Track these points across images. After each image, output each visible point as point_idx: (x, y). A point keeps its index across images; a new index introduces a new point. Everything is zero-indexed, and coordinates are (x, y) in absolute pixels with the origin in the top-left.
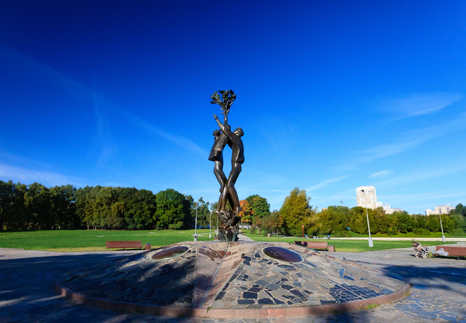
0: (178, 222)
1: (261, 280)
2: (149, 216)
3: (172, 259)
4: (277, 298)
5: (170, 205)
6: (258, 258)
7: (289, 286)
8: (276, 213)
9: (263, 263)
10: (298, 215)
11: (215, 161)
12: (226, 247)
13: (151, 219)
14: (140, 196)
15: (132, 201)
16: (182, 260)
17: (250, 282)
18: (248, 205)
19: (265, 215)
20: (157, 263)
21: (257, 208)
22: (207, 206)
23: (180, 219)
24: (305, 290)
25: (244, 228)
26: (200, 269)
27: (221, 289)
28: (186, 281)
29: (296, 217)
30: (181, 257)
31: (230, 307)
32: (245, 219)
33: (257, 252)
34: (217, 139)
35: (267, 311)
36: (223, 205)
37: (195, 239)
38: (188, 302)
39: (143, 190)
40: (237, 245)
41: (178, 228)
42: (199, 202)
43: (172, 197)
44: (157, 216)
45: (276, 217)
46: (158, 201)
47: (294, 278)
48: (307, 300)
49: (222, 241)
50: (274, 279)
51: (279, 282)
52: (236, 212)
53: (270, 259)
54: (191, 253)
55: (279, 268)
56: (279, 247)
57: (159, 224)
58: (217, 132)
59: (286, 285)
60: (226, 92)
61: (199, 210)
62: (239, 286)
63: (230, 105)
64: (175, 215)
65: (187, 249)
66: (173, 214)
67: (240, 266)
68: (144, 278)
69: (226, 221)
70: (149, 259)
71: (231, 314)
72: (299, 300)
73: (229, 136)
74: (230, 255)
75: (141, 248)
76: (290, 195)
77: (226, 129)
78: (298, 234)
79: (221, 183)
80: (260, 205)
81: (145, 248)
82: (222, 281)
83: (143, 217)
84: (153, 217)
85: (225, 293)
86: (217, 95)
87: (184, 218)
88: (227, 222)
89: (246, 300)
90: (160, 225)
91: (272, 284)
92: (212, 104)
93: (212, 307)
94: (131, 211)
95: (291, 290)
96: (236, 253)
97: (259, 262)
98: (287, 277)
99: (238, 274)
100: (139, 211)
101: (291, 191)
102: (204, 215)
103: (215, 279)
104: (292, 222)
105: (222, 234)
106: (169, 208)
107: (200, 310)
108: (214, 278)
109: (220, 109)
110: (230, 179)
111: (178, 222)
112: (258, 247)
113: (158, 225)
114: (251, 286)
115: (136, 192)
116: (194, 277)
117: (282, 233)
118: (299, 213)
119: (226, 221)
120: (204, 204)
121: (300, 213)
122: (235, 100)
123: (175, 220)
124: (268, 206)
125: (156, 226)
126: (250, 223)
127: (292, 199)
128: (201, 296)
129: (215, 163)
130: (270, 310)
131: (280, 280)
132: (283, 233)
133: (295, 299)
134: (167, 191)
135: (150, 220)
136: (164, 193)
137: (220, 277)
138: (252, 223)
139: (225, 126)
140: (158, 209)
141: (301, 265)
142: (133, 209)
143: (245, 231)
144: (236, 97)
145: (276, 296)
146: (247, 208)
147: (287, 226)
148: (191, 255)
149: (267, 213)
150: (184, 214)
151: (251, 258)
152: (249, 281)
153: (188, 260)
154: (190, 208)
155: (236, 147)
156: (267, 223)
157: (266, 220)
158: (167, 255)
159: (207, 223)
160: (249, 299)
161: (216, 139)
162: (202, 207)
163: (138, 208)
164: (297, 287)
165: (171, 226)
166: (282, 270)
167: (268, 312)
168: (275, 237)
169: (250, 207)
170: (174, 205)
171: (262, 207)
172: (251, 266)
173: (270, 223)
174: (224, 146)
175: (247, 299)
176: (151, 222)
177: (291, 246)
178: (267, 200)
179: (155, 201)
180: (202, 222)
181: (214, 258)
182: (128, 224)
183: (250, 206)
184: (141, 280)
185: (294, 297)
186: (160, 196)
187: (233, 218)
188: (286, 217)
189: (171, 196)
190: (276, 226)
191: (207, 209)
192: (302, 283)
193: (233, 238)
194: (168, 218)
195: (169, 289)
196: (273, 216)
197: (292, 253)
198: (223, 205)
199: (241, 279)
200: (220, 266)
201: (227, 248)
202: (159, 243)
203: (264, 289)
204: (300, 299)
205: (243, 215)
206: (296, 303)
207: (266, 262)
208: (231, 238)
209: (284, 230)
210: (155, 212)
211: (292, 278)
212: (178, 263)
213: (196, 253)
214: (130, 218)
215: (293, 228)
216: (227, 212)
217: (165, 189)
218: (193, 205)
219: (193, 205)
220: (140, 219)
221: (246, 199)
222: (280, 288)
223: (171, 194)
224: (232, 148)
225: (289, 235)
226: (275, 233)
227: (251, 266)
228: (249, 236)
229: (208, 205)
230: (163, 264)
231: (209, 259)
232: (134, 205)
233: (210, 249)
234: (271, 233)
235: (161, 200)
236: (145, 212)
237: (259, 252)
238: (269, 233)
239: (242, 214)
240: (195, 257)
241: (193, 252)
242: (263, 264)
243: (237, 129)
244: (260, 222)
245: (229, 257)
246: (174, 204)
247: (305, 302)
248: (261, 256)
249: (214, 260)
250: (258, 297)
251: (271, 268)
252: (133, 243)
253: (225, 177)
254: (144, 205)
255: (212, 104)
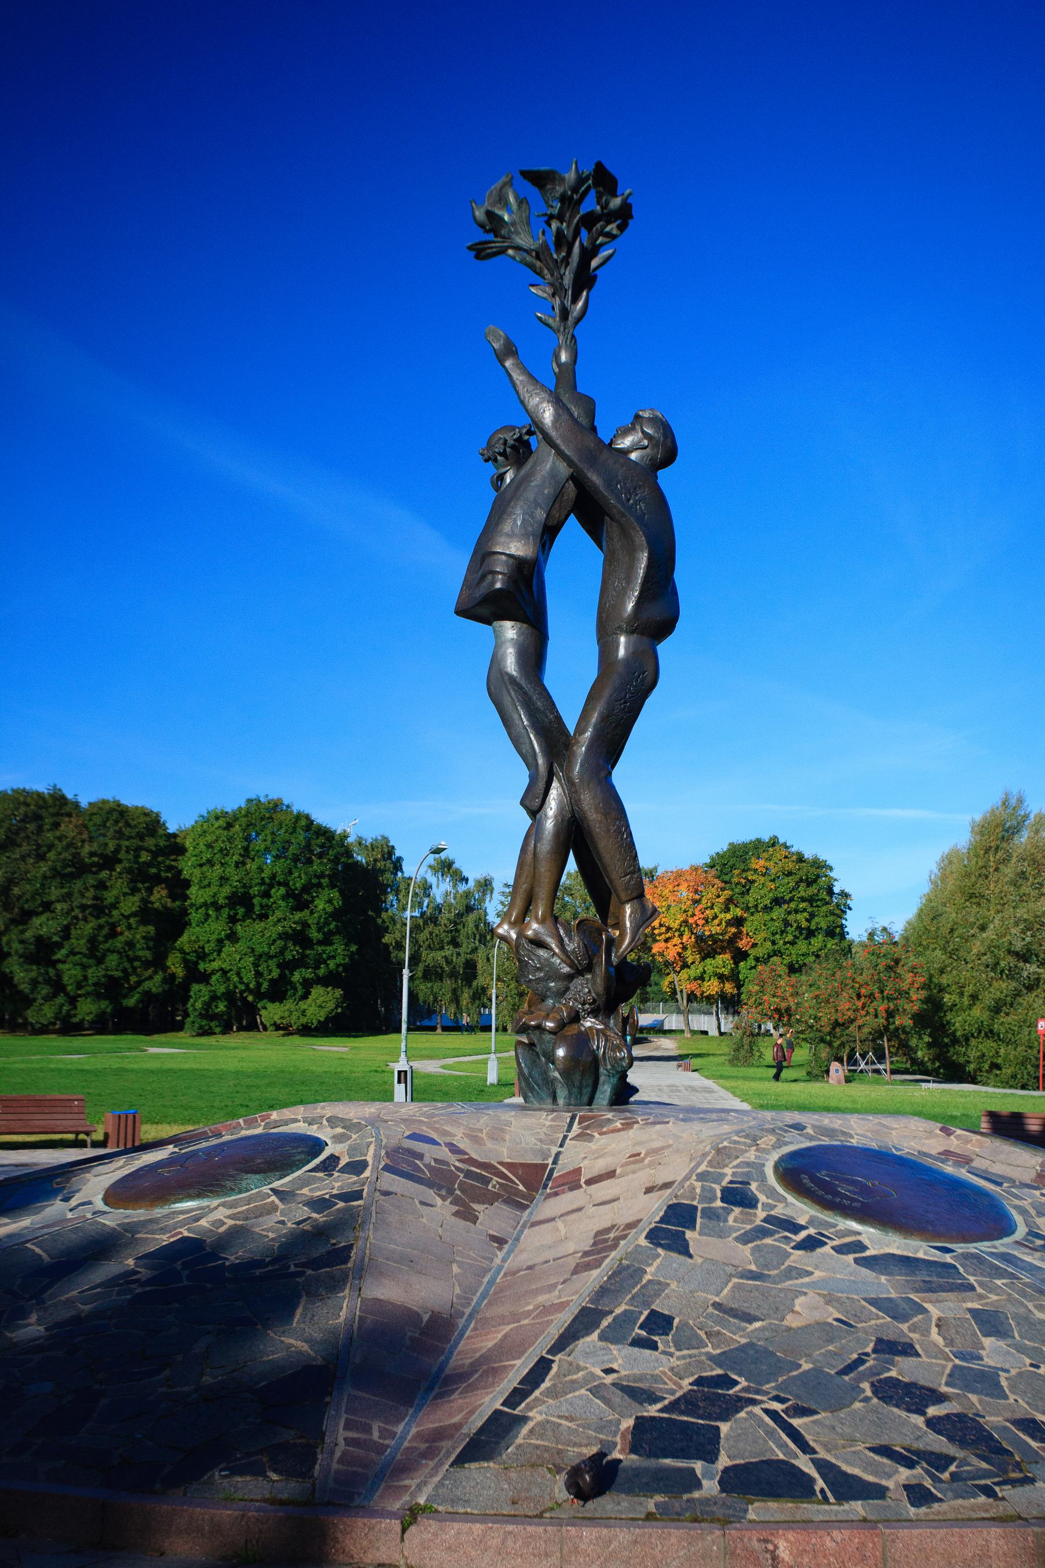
0: (313, 991)
1: (750, 1345)
2: (147, 955)
3: (224, 1205)
4: (839, 1464)
5: (267, 895)
6: (737, 1210)
7: (923, 1387)
8: (884, 949)
9: (768, 1241)
10: (1012, 960)
11: (495, 623)
12: (553, 1142)
13: (156, 972)
14: (91, 839)
15: (44, 868)
16: (278, 1216)
17: (678, 1358)
18: (722, 899)
19: (818, 956)
20: (132, 1228)
21: (774, 915)
22: (482, 900)
23: (322, 971)
24: (1018, 1415)
25: (694, 1032)
26: (381, 1273)
27: (501, 1393)
28: (292, 1341)
29: (1002, 972)
30: (273, 1198)
31: (545, 1511)
32: (703, 980)
33: (734, 1174)
34: (508, 481)
35: (771, 1542)
36: (543, 893)
37: (399, 1090)
38: (288, 1473)
39: (107, 807)
40: (619, 1130)
41: (315, 1023)
42: (432, 879)
43: (279, 845)
44: (192, 957)
45: (881, 967)
46: (197, 872)
47: (958, 1340)
48: (1031, 1481)
49: (536, 1105)
50: (830, 1341)
51: (860, 1361)
52: (622, 935)
53: (812, 1222)
54: (336, 1174)
55: (865, 1272)
56: (874, 1145)
57: (205, 1003)
58: (510, 437)
59: (906, 1380)
60: (567, 176)
61: (436, 925)
62: (609, 1379)
63: (594, 263)
64: (293, 952)
65: (316, 1146)
66: (280, 943)
67: (628, 1254)
68: (39, 1322)
69: (561, 985)
70: (90, 1203)
71: (547, 1555)
72: (980, 1478)
73: (581, 465)
74: (571, 1189)
75: (82, 1136)
76: (971, 843)
77: (565, 417)
78: (1007, 1071)
79: (529, 760)
80: (791, 900)
81: (106, 1135)
82: (509, 1348)
83: (112, 960)
84: (166, 958)
85: (523, 1419)
86: (512, 199)
87: (344, 966)
88: (568, 995)
89: (646, 1470)
90: (207, 1005)
91: (817, 1371)
92: (477, 257)
93: (435, 1506)
94: (43, 926)
95: (932, 1411)
96: (611, 1174)
97: (745, 1239)
98: (913, 1329)
99: (611, 1306)
100: (89, 928)
101: (978, 817)
102: (462, 950)
103: (468, 1333)
104: (974, 997)
105: (534, 1062)
106: (257, 908)
107: (360, 1522)
108: (466, 1327)
109: (533, 290)
110: (588, 734)
111: (309, 993)
112: (745, 1144)
113: (199, 1005)
114: (686, 1384)
115: (69, 815)
116: (342, 1319)
117: (914, 1061)
118: (1018, 946)
119: (561, 985)
120: (462, 888)
121: (1029, 950)
122: (626, 232)
123: (296, 977)
124: (838, 905)
125: (186, 1015)
126: (731, 1004)
127: (980, 864)
128: (376, 1435)
129: (497, 635)
130: (791, 1536)
131: (869, 1350)
132: (922, 1063)
133: (951, 1474)
134: (248, 814)
135: (151, 978)
136: (228, 821)
137: (503, 1320)
138: (739, 1002)
139: (557, 402)
140: (195, 916)
141: (1006, 1258)
142: (53, 912)
143: (702, 1046)
144: (634, 212)
145: (836, 1447)
146: (715, 917)
147: (948, 1022)
148: (338, 1183)
149: (831, 944)
150: (346, 945)
151: (696, 1208)
152: (672, 1350)
153: (315, 1215)
154: (379, 911)
155: (624, 532)
156: (828, 1002)
157: (825, 988)
158: (191, 1186)
159: (480, 995)
160: (668, 1461)
161: (504, 486)
162: (450, 905)
163: (83, 908)
164: (974, 1398)
165: (271, 1012)
166: (887, 1286)
167: (776, 1547)
168: (888, 1083)
169: (732, 907)
170: (290, 894)
171: (805, 910)
172: (690, 1256)
173: (845, 1004)
174: (548, 533)
175: (652, 1463)
176: (160, 990)
177: (953, 1143)
178: (831, 869)
179: (180, 872)
180: (454, 991)
181: (475, 1206)
182: (27, 1001)
183: (730, 900)
184: (22, 1331)
185: (950, 1460)
186: (209, 838)
187: (601, 970)
188: (942, 971)
189: (273, 842)
190: (881, 1021)
191: (482, 919)
192: (1007, 1371)
193: (600, 1087)
194: (256, 965)
195: (186, 1389)
196: (866, 965)
197: (955, 1185)
198: (543, 893)
199: (625, 1338)
200: (509, 1253)
201: (561, 1146)
202: (191, 1107)
203: (762, 1402)
204: (986, 1475)
205: (689, 952)
206: (956, 1497)
207: (786, 1237)
208: (589, 1089)
209: (929, 1045)
210: (180, 934)
211: (940, 1341)
212: (257, 1230)
213: (367, 1173)
214: (38, 964)
215: (980, 1032)
216: (568, 932)
217: (233, 802)
218: (397, 892)
219: (397, 892)
220: (95, 974)
221: (708, 861)
222: (866, 1400)
223: (268, 832)
224: (604, 544)
225: (955, 1073)
226: (873, 1063)
227: (690, 1256)
228: (721, 1077)
229: (484, 894)
230: (165, 1239)
231: (443, 1208)
232: (55, 893)
233: (454, 1149)
234: (852, 1060)
235: (210, 862)
236: (121, 934)
237: (747, 1174)
238: (840, 1060)
239: (685, 948)
240: (358, 1195)
241: (347, 1164)
242: (766, 1245)
243: (637, 417)
244: (784, 999)
245: (568, 1200)
246: (286, 884)
247: (1019, 1490)
248: (757, 1201)
249: (474, 1219)
250: (722, 1452)
251: (818, 1274)
252: (33, 1109)
253: (559, 718)
254: (115, 892)
255: (477, 257)
